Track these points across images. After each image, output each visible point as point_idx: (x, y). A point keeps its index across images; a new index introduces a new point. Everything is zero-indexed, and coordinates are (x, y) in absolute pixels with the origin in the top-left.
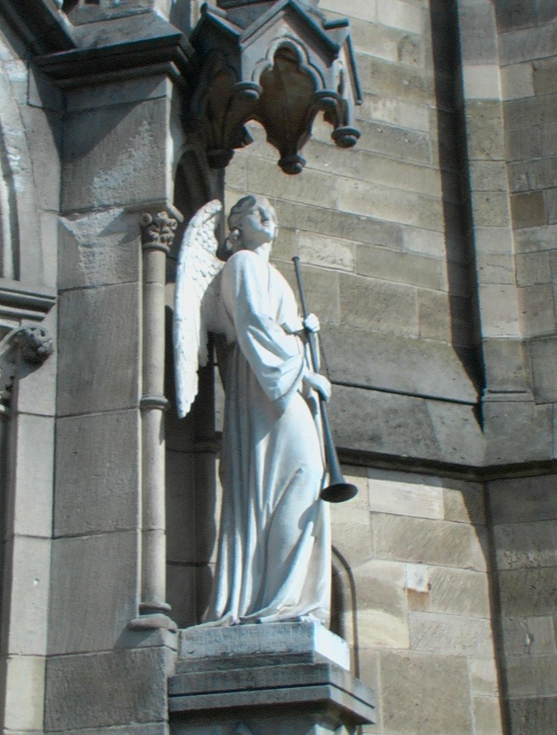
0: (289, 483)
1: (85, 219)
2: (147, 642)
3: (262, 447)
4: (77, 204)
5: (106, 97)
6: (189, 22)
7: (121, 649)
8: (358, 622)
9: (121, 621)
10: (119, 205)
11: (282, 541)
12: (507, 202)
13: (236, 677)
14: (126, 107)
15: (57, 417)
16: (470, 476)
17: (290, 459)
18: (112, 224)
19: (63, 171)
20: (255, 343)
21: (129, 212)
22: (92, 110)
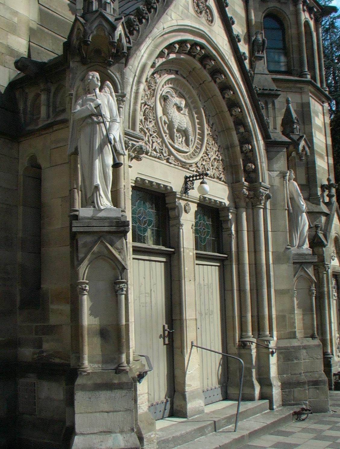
0: (304, 225)
1: (272, 172)
2: (289, 251)
3: (300, 218)
4: (271, 169)
5: (275, 149)
6: (246, 68)
7: (285, 251)
8: (128, 121)
9: (284, 247)
10: (279, 171)
11: (304, 235)
12: (264, 24)
13: (303, 257)
14: (279, 152)
15: (270, 210)
16: (182, 57)
17: (304, 219)
18: (278, 174)
19: (268, 162)
20: (300, 200)
21: (280, 173)
22: (272, 151)
